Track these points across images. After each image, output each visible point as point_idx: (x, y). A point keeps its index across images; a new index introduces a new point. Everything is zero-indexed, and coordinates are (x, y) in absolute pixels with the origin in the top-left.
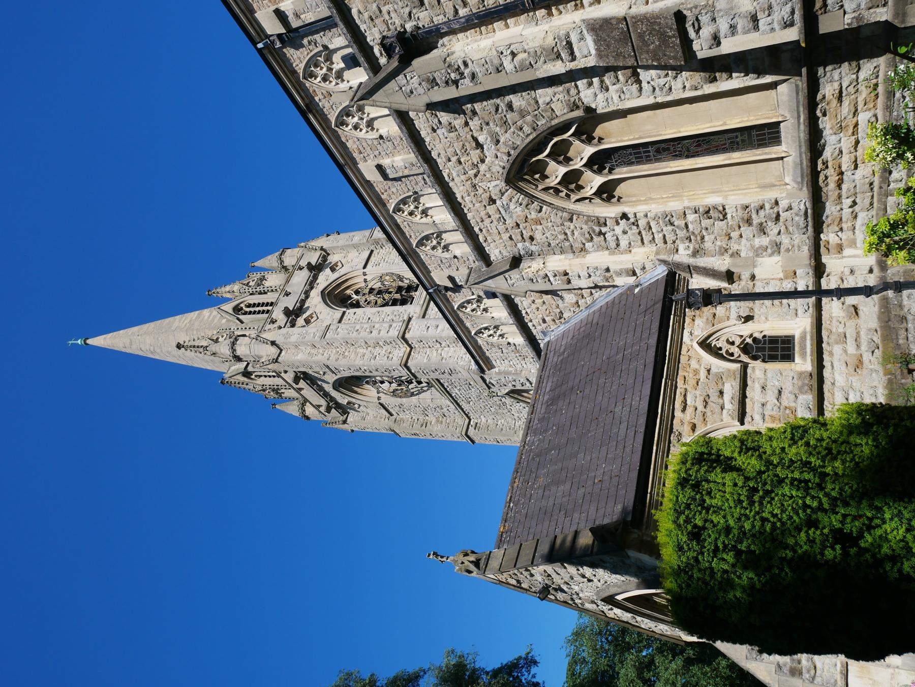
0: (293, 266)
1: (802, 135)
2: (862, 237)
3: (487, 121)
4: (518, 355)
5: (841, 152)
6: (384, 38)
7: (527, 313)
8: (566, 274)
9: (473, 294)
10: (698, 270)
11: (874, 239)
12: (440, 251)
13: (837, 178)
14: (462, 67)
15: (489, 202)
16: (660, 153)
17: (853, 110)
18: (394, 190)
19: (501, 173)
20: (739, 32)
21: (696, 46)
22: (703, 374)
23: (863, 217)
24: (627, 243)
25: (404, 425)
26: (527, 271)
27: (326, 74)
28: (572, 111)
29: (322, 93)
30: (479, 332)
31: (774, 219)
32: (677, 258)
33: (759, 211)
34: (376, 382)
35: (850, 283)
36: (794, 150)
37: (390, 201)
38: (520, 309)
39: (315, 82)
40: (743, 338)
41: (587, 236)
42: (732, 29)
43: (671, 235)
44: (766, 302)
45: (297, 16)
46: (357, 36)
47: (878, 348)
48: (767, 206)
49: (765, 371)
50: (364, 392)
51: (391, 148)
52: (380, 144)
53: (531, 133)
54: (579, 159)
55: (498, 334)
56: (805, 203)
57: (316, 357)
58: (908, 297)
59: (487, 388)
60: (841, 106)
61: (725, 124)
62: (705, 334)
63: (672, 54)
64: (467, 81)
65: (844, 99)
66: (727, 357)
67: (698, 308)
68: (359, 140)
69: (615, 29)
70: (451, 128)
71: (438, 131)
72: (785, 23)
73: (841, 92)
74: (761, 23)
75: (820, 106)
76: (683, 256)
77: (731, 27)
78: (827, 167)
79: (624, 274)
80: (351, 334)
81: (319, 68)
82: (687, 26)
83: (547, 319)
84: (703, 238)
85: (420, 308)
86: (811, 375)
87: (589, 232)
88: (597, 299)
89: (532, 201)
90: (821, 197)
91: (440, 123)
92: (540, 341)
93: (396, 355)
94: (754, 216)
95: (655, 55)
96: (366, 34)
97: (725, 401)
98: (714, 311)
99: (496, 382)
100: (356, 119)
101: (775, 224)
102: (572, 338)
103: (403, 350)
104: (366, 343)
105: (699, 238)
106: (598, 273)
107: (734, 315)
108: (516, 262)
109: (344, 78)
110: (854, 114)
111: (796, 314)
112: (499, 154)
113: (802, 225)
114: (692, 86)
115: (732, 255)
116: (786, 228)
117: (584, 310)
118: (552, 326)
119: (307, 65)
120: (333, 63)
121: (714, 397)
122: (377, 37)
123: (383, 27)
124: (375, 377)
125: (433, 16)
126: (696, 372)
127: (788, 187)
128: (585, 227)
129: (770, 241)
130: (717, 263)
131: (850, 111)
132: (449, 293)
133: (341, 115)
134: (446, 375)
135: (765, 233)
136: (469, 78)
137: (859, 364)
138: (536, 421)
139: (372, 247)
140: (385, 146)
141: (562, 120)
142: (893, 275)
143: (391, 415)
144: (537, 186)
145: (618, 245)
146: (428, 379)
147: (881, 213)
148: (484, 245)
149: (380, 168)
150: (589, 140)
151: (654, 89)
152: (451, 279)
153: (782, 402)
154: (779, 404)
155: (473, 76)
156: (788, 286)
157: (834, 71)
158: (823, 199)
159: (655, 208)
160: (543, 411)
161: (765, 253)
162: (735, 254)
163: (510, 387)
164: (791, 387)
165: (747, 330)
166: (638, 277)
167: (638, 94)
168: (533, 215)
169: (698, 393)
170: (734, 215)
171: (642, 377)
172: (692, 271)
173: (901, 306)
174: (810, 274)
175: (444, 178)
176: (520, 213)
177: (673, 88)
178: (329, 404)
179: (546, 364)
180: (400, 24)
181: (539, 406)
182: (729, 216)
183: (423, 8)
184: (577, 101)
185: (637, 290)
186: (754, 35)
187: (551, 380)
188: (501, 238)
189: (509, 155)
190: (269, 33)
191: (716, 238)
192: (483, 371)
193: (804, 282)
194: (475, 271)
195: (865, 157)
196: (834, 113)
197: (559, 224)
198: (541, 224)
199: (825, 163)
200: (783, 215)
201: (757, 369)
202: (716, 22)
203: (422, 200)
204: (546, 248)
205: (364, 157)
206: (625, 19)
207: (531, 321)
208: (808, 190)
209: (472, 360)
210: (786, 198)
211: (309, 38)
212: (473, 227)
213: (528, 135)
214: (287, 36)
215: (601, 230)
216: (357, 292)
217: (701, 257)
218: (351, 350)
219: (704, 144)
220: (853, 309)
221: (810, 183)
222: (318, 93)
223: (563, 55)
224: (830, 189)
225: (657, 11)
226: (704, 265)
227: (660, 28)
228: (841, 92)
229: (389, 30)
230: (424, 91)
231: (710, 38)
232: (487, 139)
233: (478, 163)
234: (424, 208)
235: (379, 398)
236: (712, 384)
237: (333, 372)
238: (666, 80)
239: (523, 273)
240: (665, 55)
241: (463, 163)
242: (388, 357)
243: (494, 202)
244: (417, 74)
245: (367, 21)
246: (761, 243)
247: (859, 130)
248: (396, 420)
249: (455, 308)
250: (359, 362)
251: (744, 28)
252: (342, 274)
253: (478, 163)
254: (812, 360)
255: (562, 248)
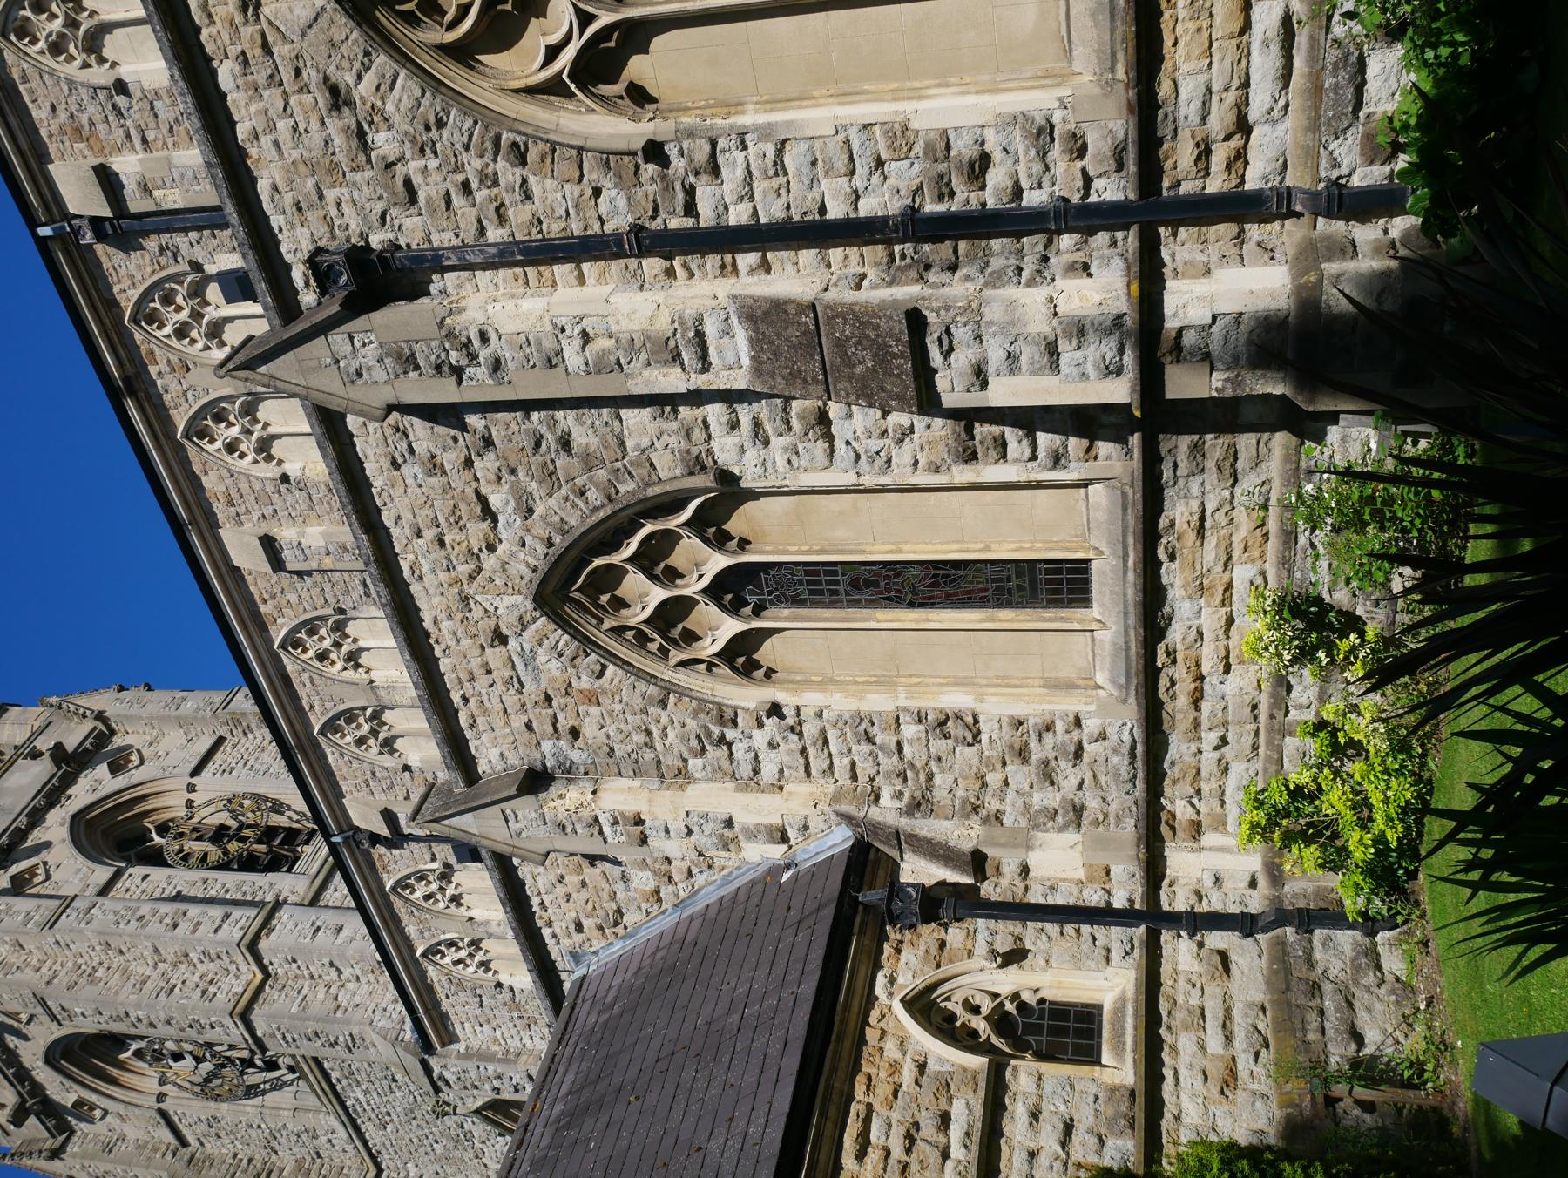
0: (16, 747)
1: (1130, 592)
2: (1237, 812)
3: (512, 465)
4: (515, 1015)
5: (1200, 634)
6: (319, 251)
7: (542, 903)
8: (639, 821)
9: (434, 859)
10: (916, 843)
11: (1260, 817)
12: (375, 750)
13: (1193, 686)
14: (476, 343)
15: (493, 640)
16: (859, 589)
17: (1224, 558)
18: (293, 598)
19: (527, 579)
20: (1024, 370)
21: (941, 382)
22: (908, 1074)
23: (1238, 772)
24: (776, 771)
25: (212, 1172)
26: (553, 804)
27: (185, 324)
28: (691, 473)
29: (169, 361)
30: (433, 951)
31: (1071, 756)
32: (875, 813)
33: (1044, 735)
34: (161, 1054)
35: (1215, 902)
36: (1114, 619)
37: (279, 621)
38: (529, 893)
39: (158, 334)
40: (999, 1000)
41: (694, 743)
42: (1010, 361)
43: (866, 765)
44: (1048, 926)
45: (146, 189)
46: (262, 240)
47: (1267, 1047)
48: (1060, 727)
49: (1040, 1079)
50: (126, 1078)
51: (302, 506)
52: (279, 492)
53: (603, 506)
54: (695, 576)
55: (477, 959)
56: (1132, 729)
57: (18, 974)
58: (1323, 945)
59: (432, 1091)
60: (1202, 545)
61: (987, 549)
62: (921, 982)
63: (895, 390)
64: (480, 373)
65: (1207, 534)
66: (965, 1039)
67: (912, 927)
68: (232, 476)
69: (793, 324)
70: (435, 466)
71: (405, 469)
72: (1107, 368)
73: (1202, 519)
74: (1063, 360)
75: (1164, 541)
76: (887, 811)
77: (1009, 357)
78: (1174, 662)
79: (762, 837)
80: (122, 926)
81: (45, 16)
82: (928, 340)
83: (586, 923)
84: (930, 777)
85: (307, 882)
86: (1132, 1093)
87: (698, 736)
88: (700, 889)
89: (585, 651)
90: (1161, 721)
91: (412, 451)
92: (564, 976)
93: (226, 988)
94: (1033, 744)
95: (864, 387)
96: (280, 237)
97: (952, 1141)
98: (942, 935)
99: (454, 1078)
100: (235, 431)
101: (1074, 766)
102: (636, 973)
103: (244, 979)
104: (156, 951)
105: (922, 777)
106: (708, 828)
107: (981, 948)
108: (535, 781)
109: (225, 337)
110: (1226, 566)
111: (1108, 959)
112: (528, 540)
113: (1125, 770)
114: (930, 463)
115: (985, 821)
116: (1094, 777)
117: (670, 910)
118: (595, 942)
119: (146, 296)
120: (208, 304)
121: (928, 1129)
122: (304, 247)
123: (322, 231)
124: (162, 1041)
125: (432, 230)
126: (895, 1067)
127: (1101, 692)
128: (692, 724)
129: (1063, 799)
130: (956, 833)
131: (1217, 557)
132: (381, 849)
133: (202, 415)
134: (340, 1050)
135: (1052, 783)
136: (487, 368)
137: (1230, 1080)
138: (526, 1167)
139: (223, 731)
140: (289, 499)
141: (668, 488)
142: (1295, 896)
143: (183, 1143)
144: (601, 621)
145: (756, 772)
146: (293, 1057)
147: (1272, 769)
148: (468, 734)
149: (269, 545)
150: (720, 541)
151: (858, 457)
152: (389, 816)
153: (1072, 1152)
154: (1064, 1156)
155: (497, 365)
156: (1094, 898)
157: (1191, 478)
158: (1165, 726)
159: (840, 703)
160: (546, 1141)
161: (1050, 824)
162: (993, 819)
163: (485, 1096)
164: (1090, 1118)
165: (1007, 981)
166: (790, 847)
167: (826, 463)
168: (585, 683)
169: (895, 1116)
170: (994, 737)
171: (776, 1069)
172: (904, 846)
173: (1310, 962)
174: (1138, 876)
175: (402, 571)
176: (556, 673)
177: (894, 460)
178: (24, 1101)
179: (570, 1029)
180: (358, 231)
181: (539, 1130)
182: (984, 737)
183: (414, 210)
184: (704, 455)
185: (786, 876)
186: (1050, 381)
187: (574, 1067)
188: (508, 724)
189: (550, 543)
190: (72, 209)
191: (956, 781)
192: (428, 1047)
193: (1125, 890)
194: (440, 792)
195: (1244, 649)
196: (1190, 557)
197: (637, 709)
198: (599, 704)
199: (1171, 654)
200: (1090, 749)
201: (1024, 1075)
202: (981, 342)
203: (351, 629)
204: (602, 759)
205: (238, 515)
206: (813, 307)
207: (550, 924)
208: (1138, 704)
209: (408, 1020)
210: (1097, 714)
211: (165, 238)
212: (449, 691)
213: (596, 509)
214: (112, 226)
215: (723, 736)
216: (163, 829)
217: (923, 817)
218: (114, 966)
219: (945, 583)
220: (1217, 960)
221: (1142, 690)
222: (158, 358)
223: (685, 356)
224: (1178, 706)
225: (875, 302)
226: (929, 835)
227: (877, 336)
228: (1202, 519)
229: (334, 238)
230: (386, 377)
231: (970, 370)
232: (507, 503)
233: (480, 550)
234: (354, 647)
235: (161, 1097)
236: (926, 1098)
237: (54, 1018)
238: (881, 443)
239: (546, 810)
240: (882, 389)
241: (448, 546)
242: (204, 992)
243: (504, 640)
244: (377, 338)
245: (288, 210)
246: (1046, 803)
247: (1235, 598)
248: (192, 1157)
249: (388, 887)
250: (127, 997)
251: (1033, 364)
252: (134, 781)
253: (480, 550)
254: (1135, 1061)
255: (637, 762)
